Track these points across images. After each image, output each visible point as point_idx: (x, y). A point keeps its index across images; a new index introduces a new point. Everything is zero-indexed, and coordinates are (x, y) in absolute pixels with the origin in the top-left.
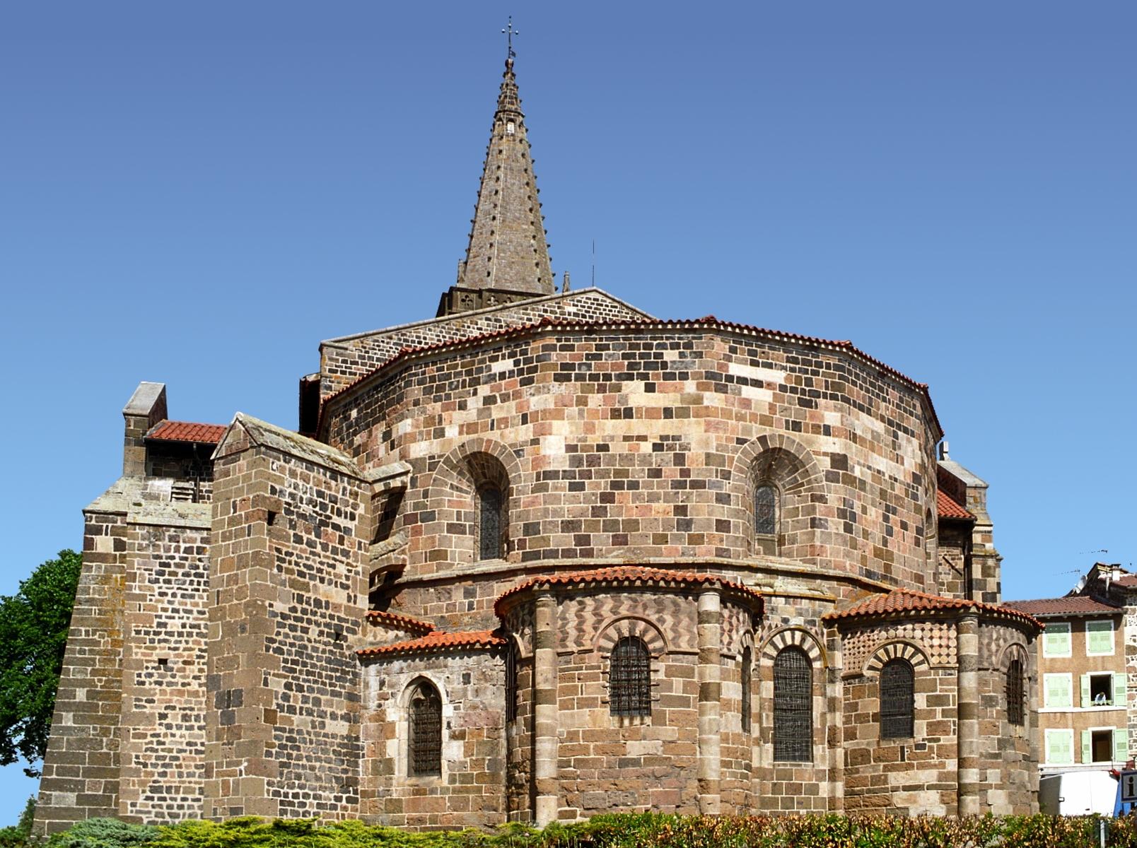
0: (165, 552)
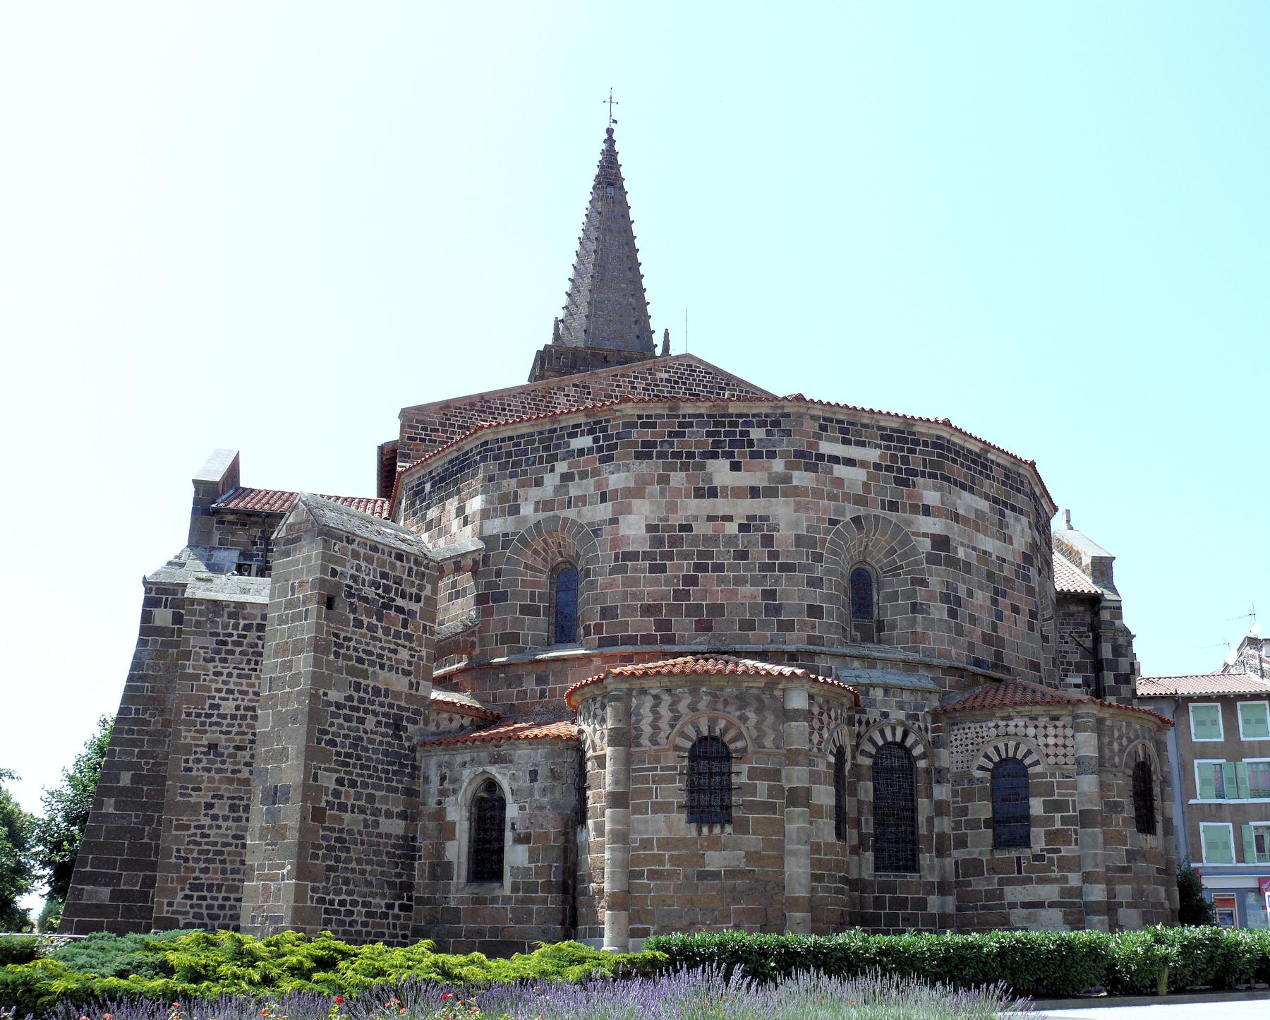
0: (223, 629)
